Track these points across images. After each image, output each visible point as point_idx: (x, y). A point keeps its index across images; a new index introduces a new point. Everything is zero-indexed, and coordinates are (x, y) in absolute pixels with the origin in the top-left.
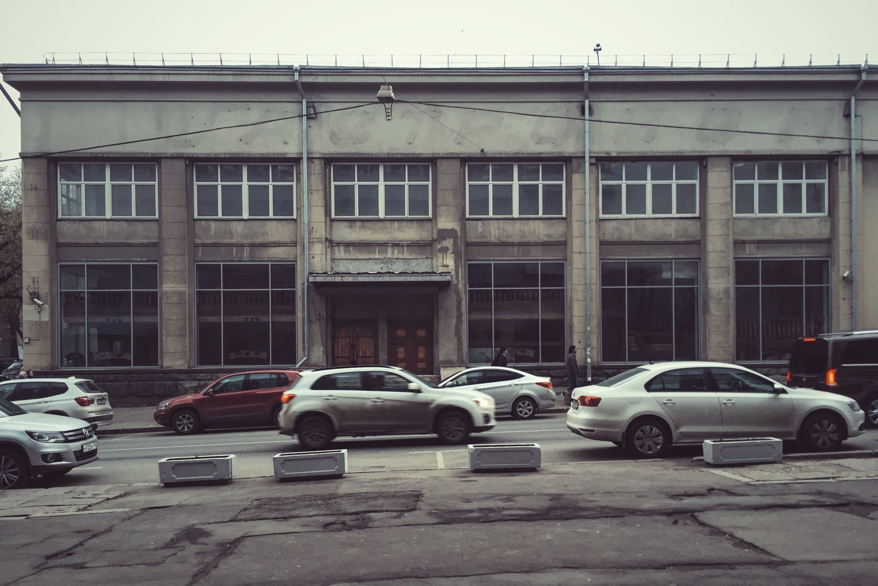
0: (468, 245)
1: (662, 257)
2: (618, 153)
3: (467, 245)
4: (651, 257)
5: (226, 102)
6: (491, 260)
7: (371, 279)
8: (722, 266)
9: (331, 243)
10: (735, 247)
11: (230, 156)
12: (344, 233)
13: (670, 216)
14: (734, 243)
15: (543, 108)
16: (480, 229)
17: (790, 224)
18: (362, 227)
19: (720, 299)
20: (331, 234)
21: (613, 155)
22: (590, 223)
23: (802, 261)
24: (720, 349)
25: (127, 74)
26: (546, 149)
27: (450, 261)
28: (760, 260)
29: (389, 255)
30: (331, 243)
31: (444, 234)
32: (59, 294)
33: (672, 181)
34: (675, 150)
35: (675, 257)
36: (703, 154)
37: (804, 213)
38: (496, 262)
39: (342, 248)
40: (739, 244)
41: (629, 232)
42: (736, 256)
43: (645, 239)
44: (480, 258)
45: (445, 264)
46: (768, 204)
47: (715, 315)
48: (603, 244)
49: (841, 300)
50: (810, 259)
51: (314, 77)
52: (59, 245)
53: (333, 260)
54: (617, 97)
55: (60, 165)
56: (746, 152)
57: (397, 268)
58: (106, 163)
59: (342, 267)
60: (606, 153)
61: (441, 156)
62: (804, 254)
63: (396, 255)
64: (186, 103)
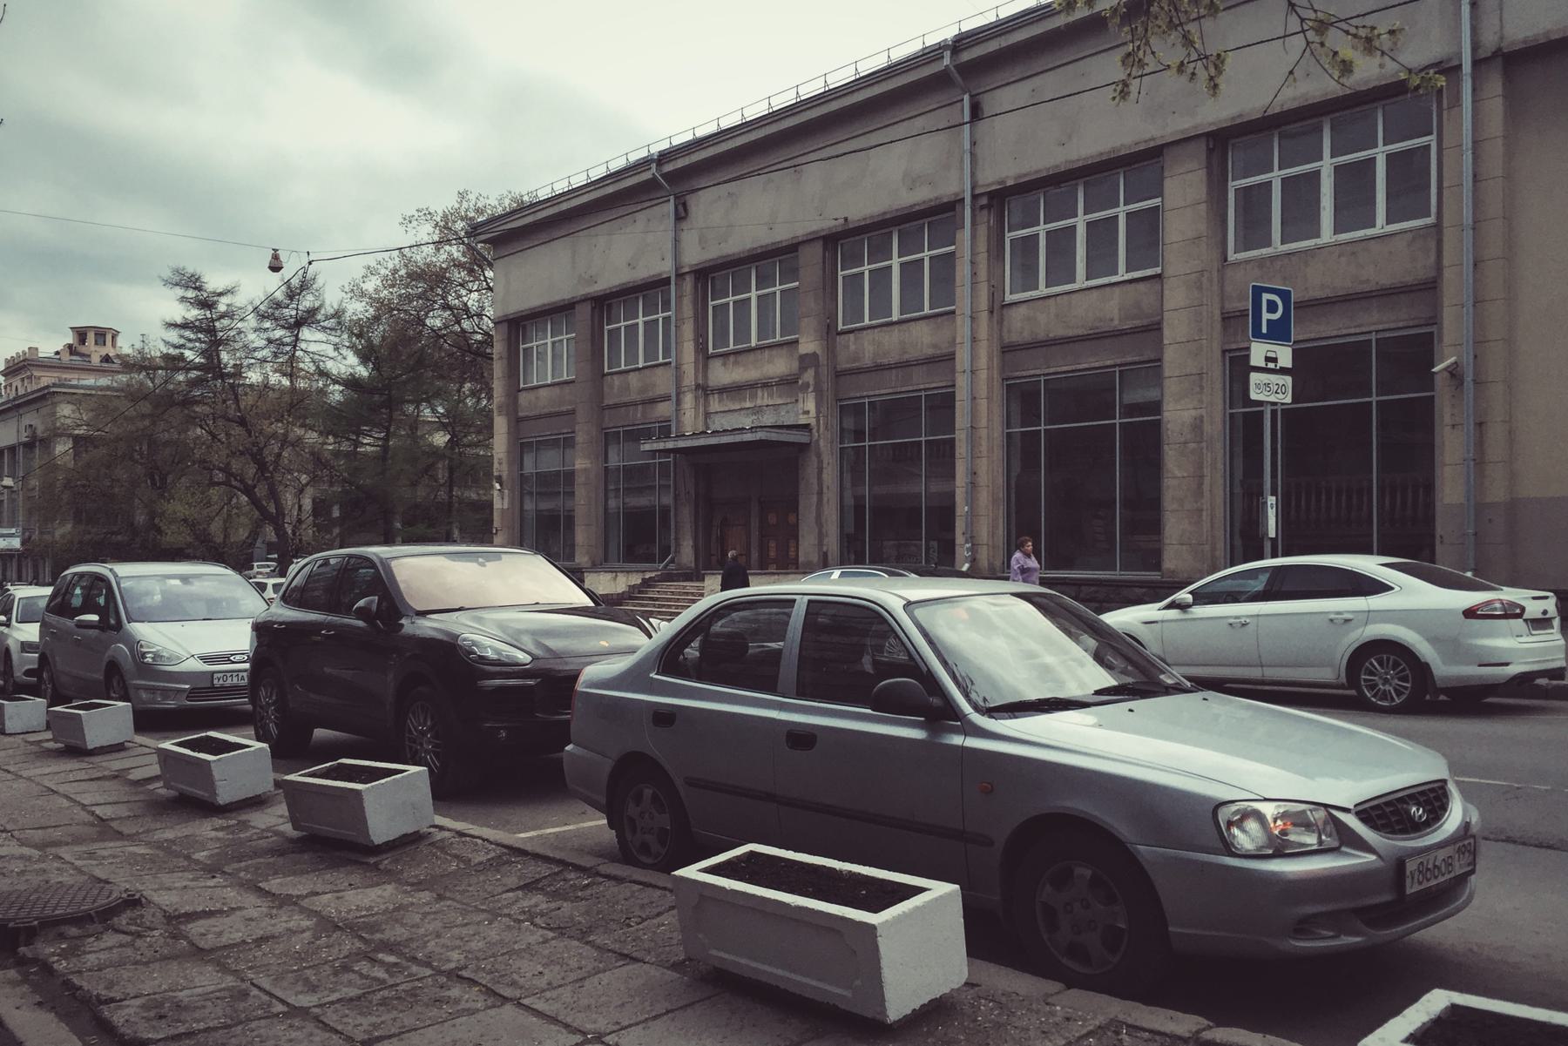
0: (839, 374)
1: (1097, 365)
2: (1016, 178)
3: (837, 376)
4: (1081, 367)
5: (916, 116)
6: (864, 397)
7: (748, 437)
8: (1188, 371)
9: (704, 390)
10: (1225, 328)
11: (764, 250)
12: (722, 374)
13: (1114, 279)
14: (1224, 319)
15: (919, 124)
16: (852, 347)
17: (1343, 259)
18: (736, 363)
19: (1185, 443)
20: (705, 376)
21: (1010, 183)
22: (1474, 229)
23: (1370, 341)
24: (1184, 547)
25: (543, 209)
26: (921, 196)
27: (811, 405)
28: (1042, 378)
29: (759, 402)
30: (704, 390)
31: (807, 361)
32: (1228, 418)
33: (1076, 219)
34: (617, 282)
35: (1118, 361)
36: (1152, 144)
37: (1381, 226)
38: (1380, 336)
39: (716, 396)
40: (1008, 349)
41: (1047, 324)
42: (1227, 347)
43: (1070, 333)
44: (852, 395)
45: (806, 409)
46: (1301, 215)
47: (1175, 477)
48: (1008, 349)
49: (1447, 429)
50: (1387, 335)
51: (673, 162)
52: (519, 420)
53: (707, 415)
54: (1018, 72)
55: (1233, 145)
56: (1233, 119)
57: (768, 419)
58: (1324, 118)
59: (719, 423)
60: (999, 183)
61: (800, 239)
62: (1372, 323)
63: (766, 402)
64: (1081, 62)
